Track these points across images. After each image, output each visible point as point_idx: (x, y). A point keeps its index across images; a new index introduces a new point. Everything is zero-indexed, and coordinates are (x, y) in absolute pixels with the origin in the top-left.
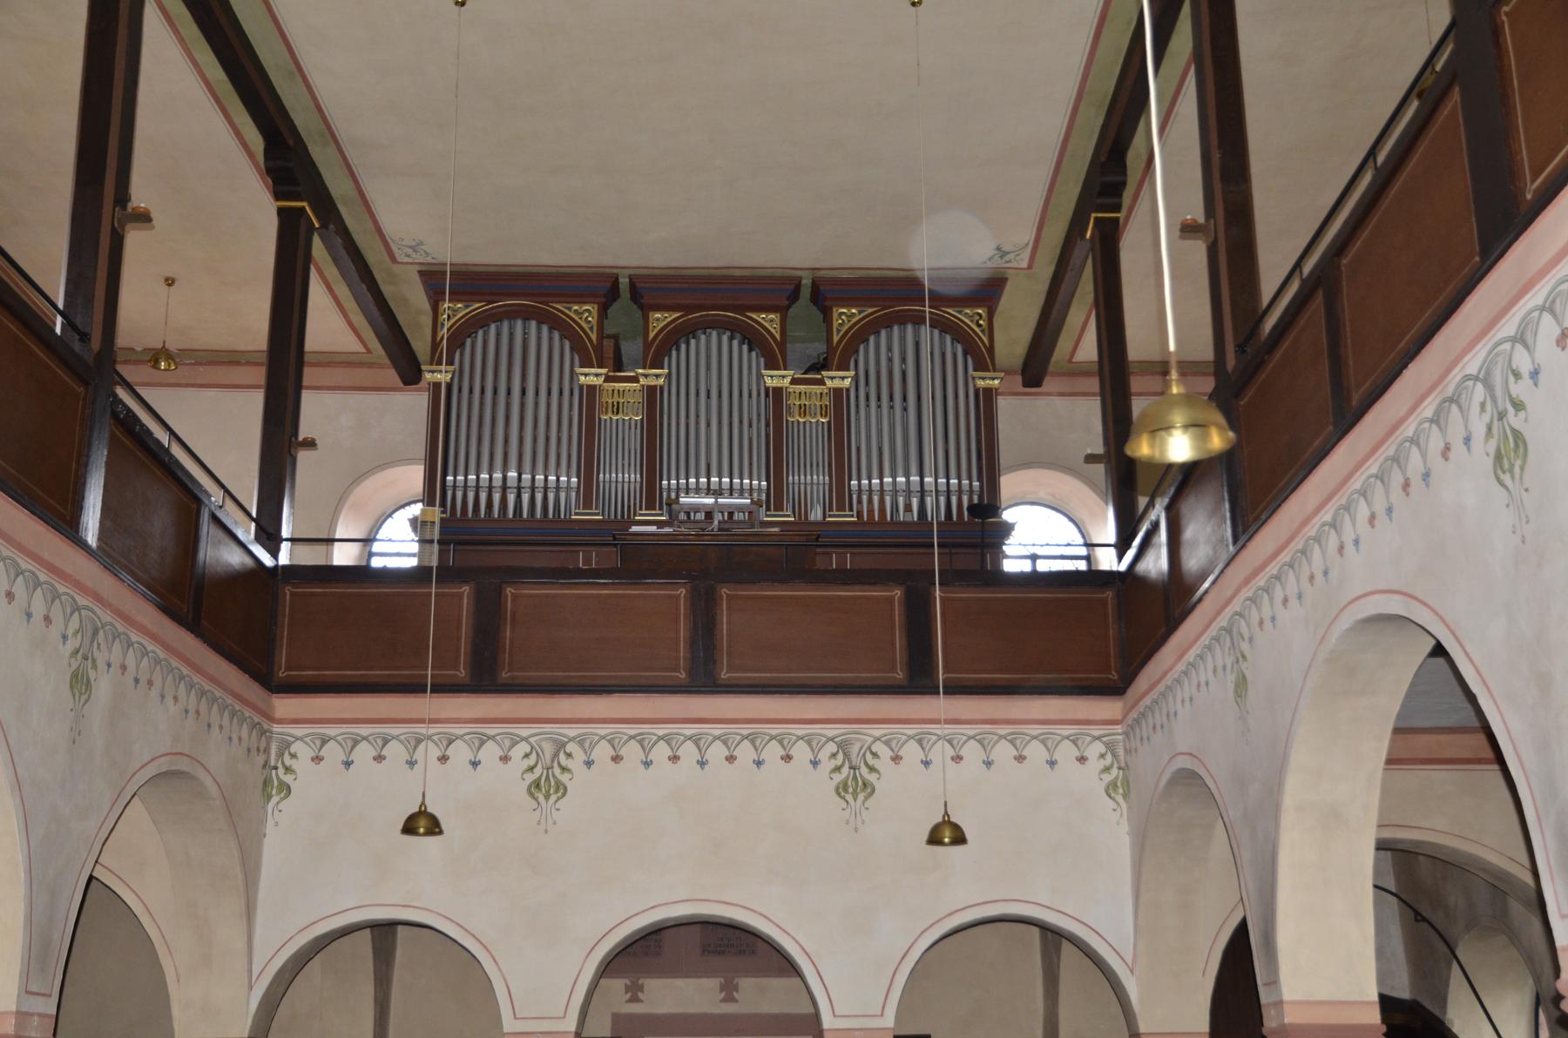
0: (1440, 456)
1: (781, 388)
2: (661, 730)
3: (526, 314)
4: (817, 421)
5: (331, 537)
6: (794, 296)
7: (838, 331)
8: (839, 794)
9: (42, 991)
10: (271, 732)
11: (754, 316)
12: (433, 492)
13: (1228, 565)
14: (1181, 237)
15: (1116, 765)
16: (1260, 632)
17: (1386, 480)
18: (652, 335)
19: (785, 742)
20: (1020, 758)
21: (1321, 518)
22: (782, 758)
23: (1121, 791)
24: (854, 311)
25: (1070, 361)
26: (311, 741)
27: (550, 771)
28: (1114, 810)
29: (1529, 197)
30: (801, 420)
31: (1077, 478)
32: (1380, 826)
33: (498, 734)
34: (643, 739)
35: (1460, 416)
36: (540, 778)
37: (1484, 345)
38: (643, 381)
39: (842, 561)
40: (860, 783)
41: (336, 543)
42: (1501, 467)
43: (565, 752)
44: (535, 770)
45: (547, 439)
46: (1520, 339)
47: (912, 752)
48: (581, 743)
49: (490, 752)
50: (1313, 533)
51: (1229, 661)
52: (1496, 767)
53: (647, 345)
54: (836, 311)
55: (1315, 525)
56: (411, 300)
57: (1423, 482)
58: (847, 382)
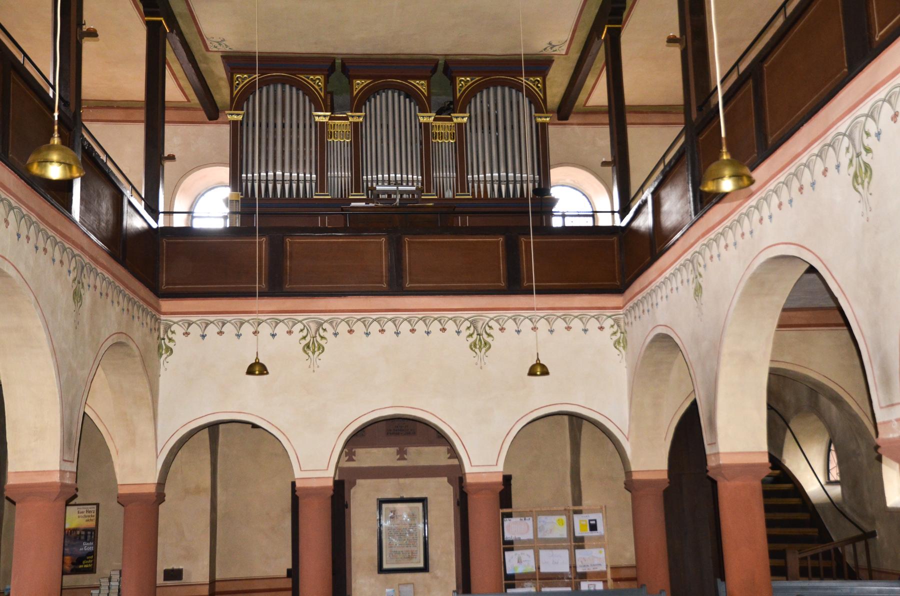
0: (822, 174)
1: (428, 123)
2: (375, 316)
3: (283, 81)
4: (449, 142)
5: (171, 211)
6: (434, 70)
7: (460, 90)
8: (472, 349)
9: (70, 460)
10: (160, 320)
11: (412, 82)
12: (235, 181)
13: (691, 226)
14: (667, 46)
15: (619, 331)
16: (711, 262)
17: (789, 185)
18: (355, 93)
19: (442, 321)
20: (568, 328)
21: (749, 203)
22: (441, 330)
23: (622, 345)
24: (468, 79)
25: (584, 105)
26: (182, 324)
27: (315, 339)
28: (619, 355)
29: (877, 39)
30: (440, 141)
31: (587, 171)
32: (772, 361)
33: (286, 319)
34: (365, 321)
35: (834, 154)
36: (309, 343)
37: (850, 118)
38: (350, 119)
39: (464, 222)
40: (483, 342)
41: (174, 214)
42: (857, 182)
43: (322, 328)
44: (307, 338)
45: (298, 153)
46: (871, 115)
47: (510, 326)
48: (331, 323)
49: (281, 329)
50: (744, 211)
51: (691, 277)
52: (845, 328)
53: (353, 99)
54: (458, 79)
55: (746, 207)
56: (217, 72)
57: (812, 188)
58: (465, 120)
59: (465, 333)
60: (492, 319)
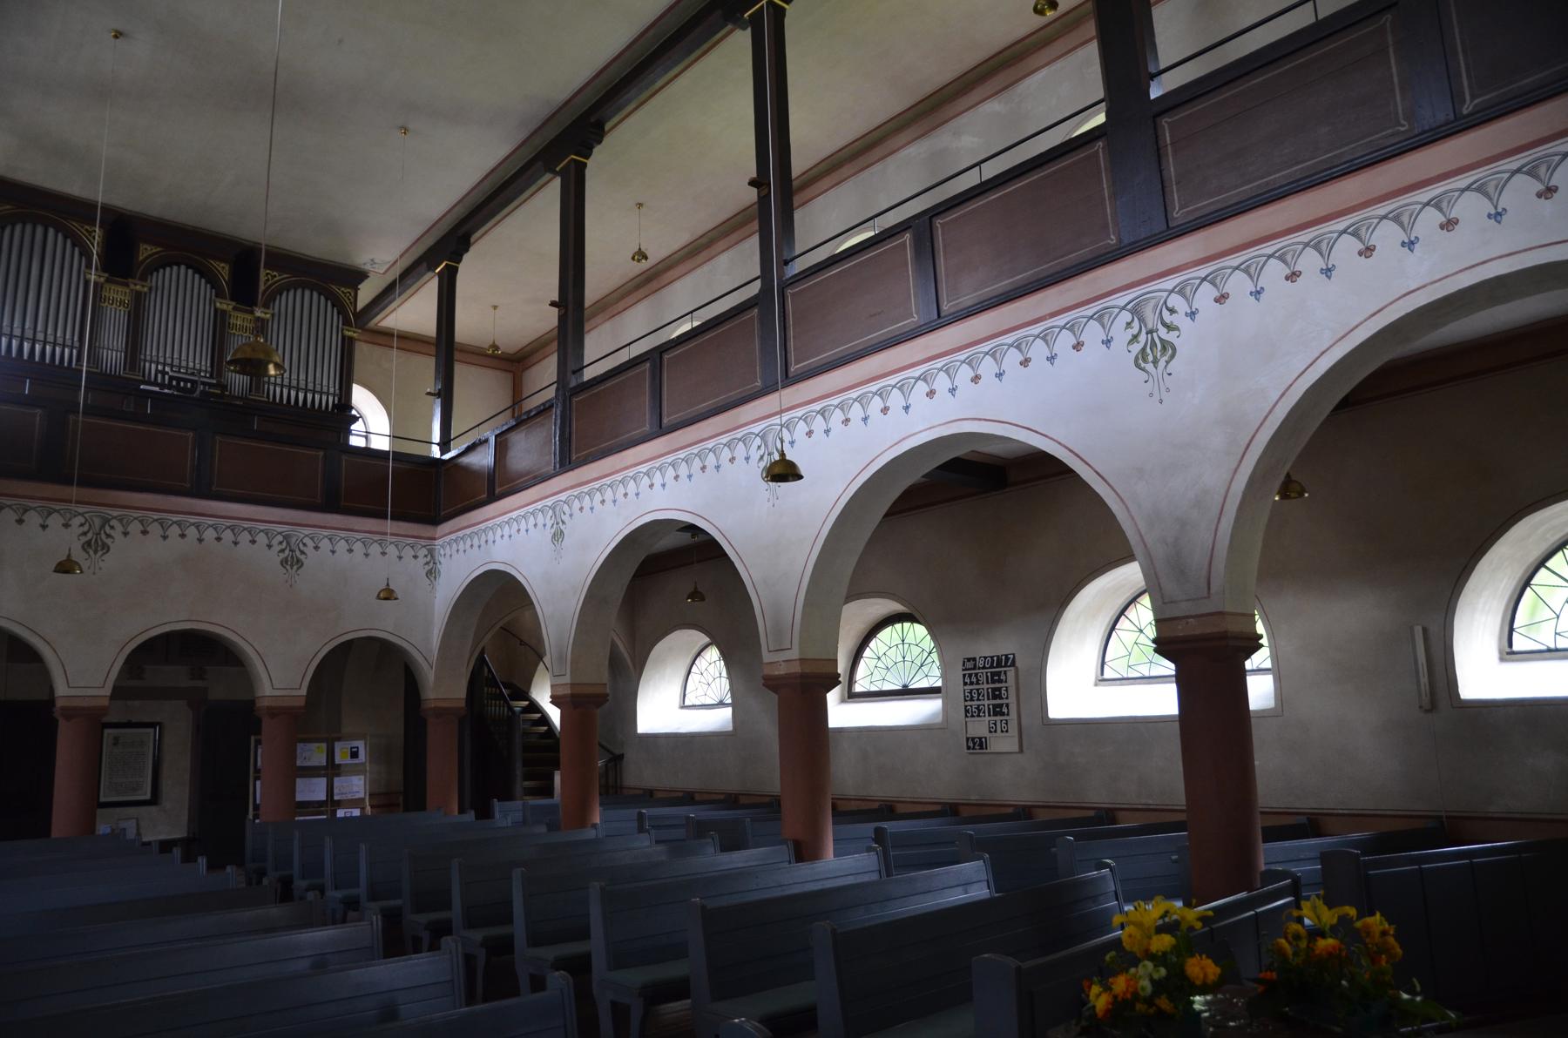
8: (282, 565)
20: (384, 554)
36: (91, 540)
48: (121, 521)
49: (55, 521)
59: (277, 548)
60: (307, 536)
